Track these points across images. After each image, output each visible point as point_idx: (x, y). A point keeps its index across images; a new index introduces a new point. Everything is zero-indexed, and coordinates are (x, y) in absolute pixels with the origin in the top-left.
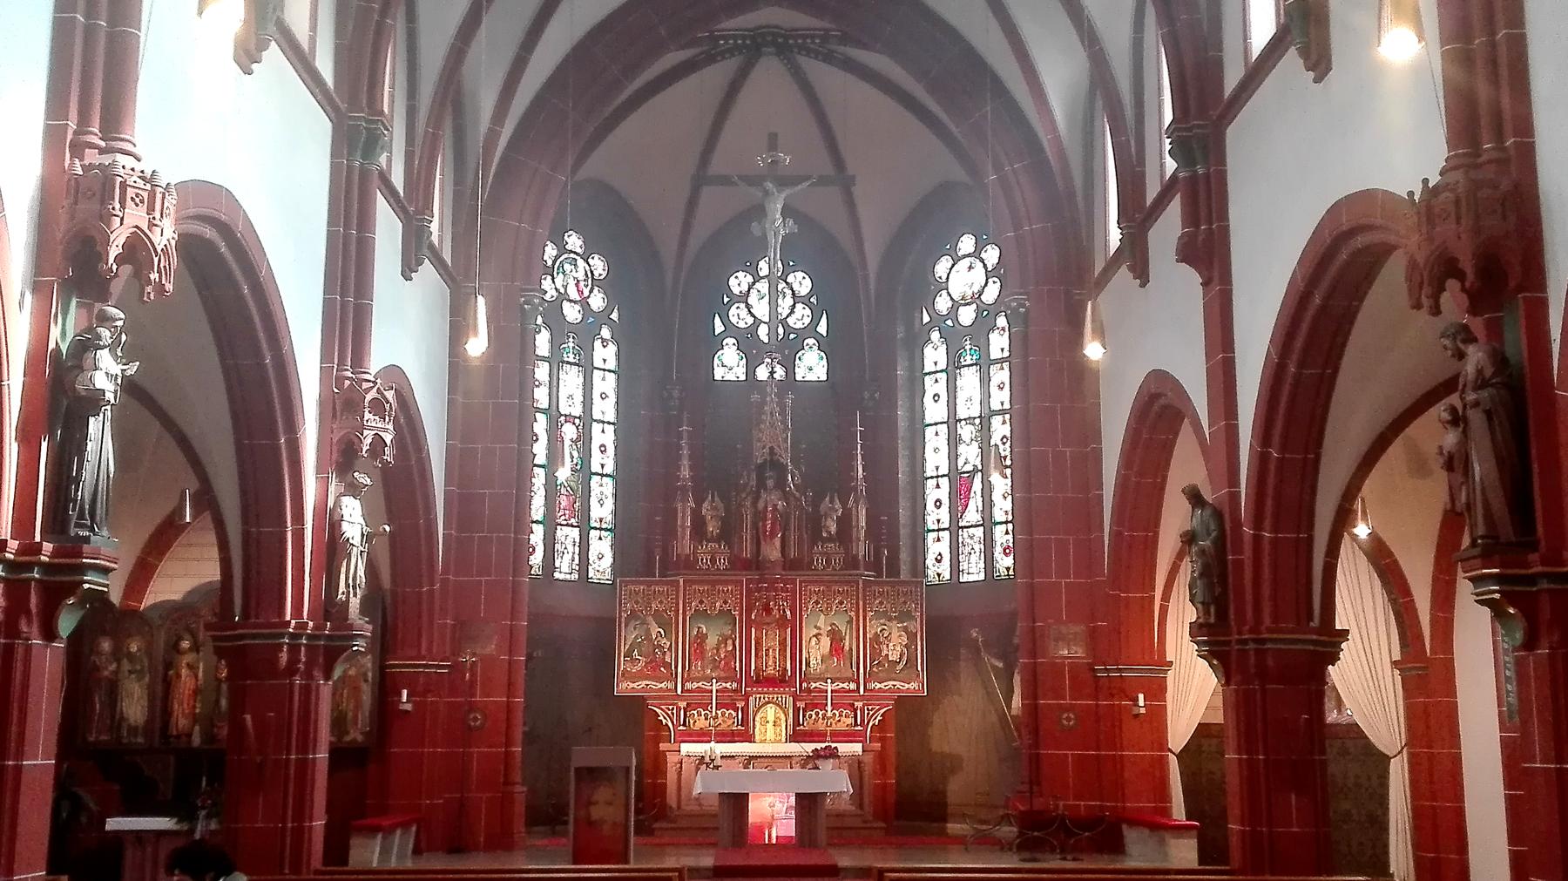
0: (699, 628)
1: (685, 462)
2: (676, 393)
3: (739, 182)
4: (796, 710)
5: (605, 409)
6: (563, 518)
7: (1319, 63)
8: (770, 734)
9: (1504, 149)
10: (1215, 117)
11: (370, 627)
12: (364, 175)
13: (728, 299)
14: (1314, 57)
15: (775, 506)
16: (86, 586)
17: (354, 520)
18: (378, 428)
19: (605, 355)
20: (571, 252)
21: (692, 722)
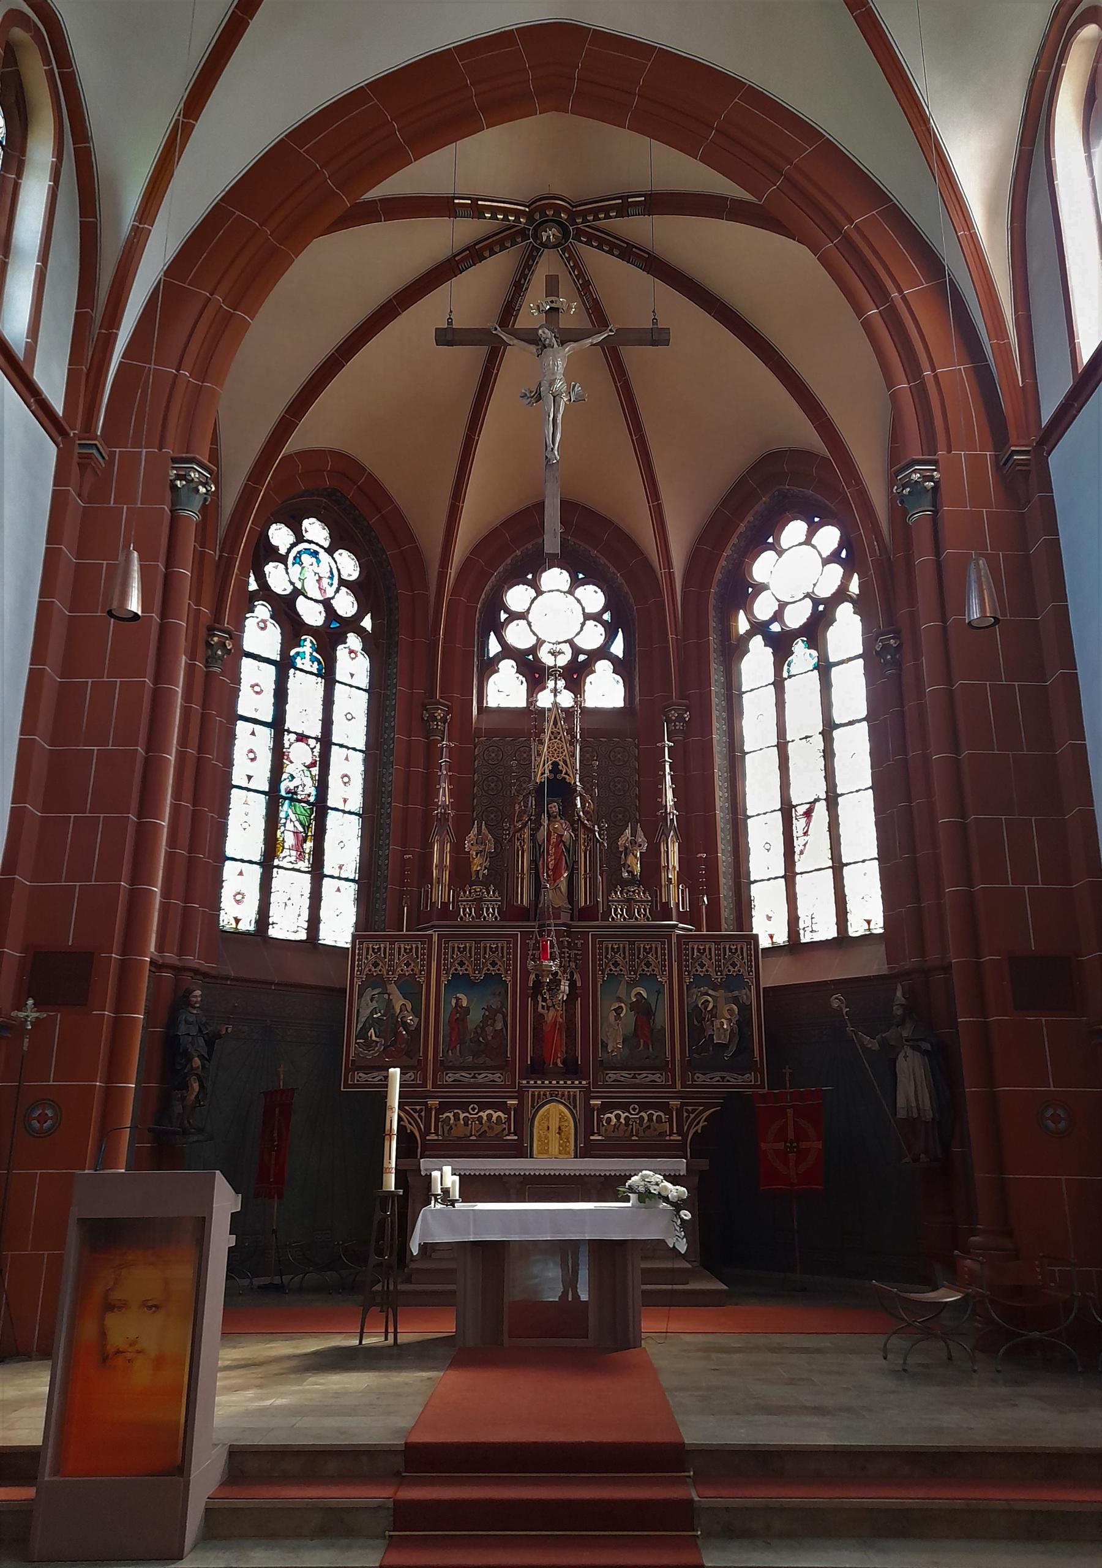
0: (458, 999)
2: (439, 714)
4: (589, 1110)
6: (288, 859)
8: (554, 1148)
13: (507, 616)
21: (446, 1128)
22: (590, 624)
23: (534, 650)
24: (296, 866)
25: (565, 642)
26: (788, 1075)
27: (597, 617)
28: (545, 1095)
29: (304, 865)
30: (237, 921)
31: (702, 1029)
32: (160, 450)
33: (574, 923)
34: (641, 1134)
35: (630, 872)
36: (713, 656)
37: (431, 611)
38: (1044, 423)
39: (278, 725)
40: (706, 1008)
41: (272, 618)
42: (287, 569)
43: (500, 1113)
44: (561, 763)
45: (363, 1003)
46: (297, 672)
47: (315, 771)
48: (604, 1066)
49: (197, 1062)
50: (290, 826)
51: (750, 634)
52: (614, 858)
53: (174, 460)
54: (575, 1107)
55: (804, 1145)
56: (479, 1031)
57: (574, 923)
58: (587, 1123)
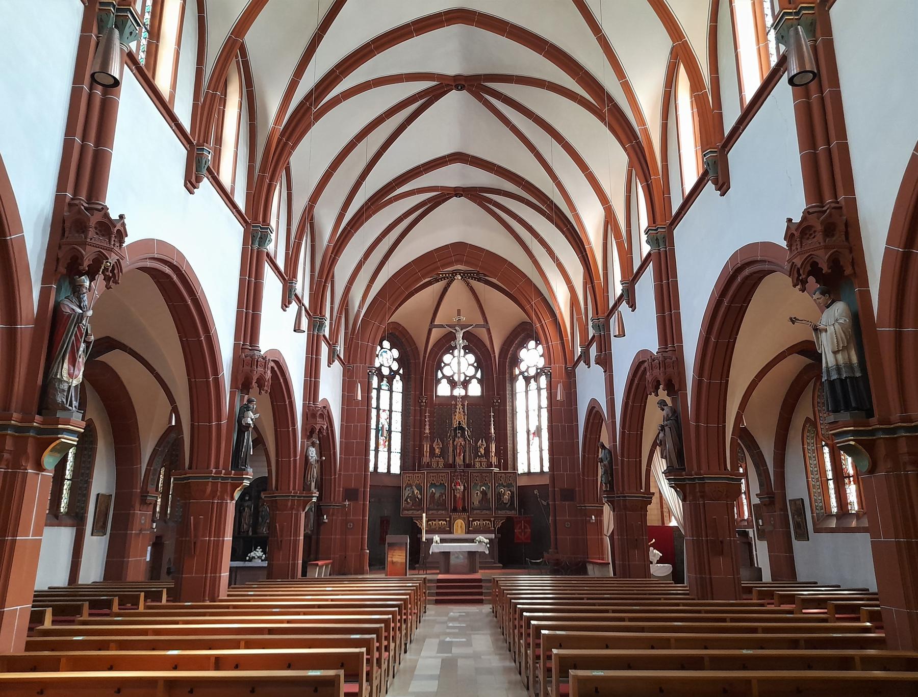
1: (427, 427)
2: (424, 401)
4: (469, 521)
5: (398, 406)
7: (723, 186)
9: (838, 203)
10: (720, 147)
11: (318, 493)
12: (259, 253)
14: (720, 182)
15: (461, 443)
16: (244, 484)
17: (313, 453)
18: (322, 424)
19: (398, 385)
22: (471, 367)
23: (452, 376)
27: (472, 365)
35: (481, 453)
38: (674, 213)
43: (444, 522)
47: (388, 420)
48: (473, 509)
52: (477, 449)
58: (468, 525)
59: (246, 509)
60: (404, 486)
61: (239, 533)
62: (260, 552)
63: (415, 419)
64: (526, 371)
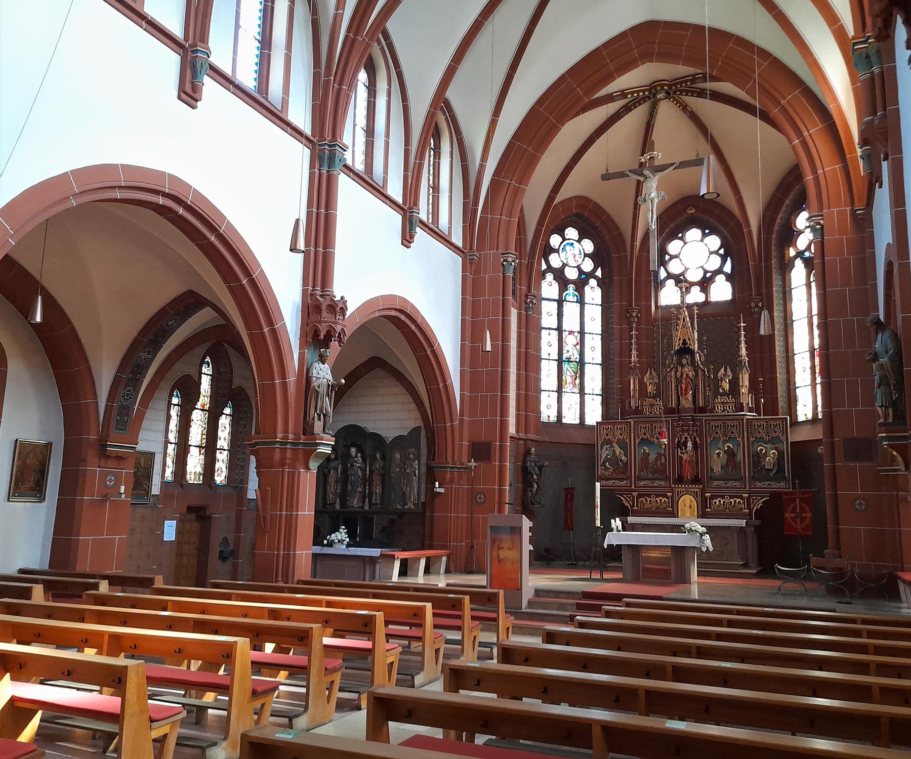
2: (634, 314)
3: (630, 174)
8: (688, 514)
13: (669, 257)
19: (593, 293)
20: (569, 239)
21: (642, 505)
22: (714, 255)
24: (573, 391)
25: (700, 267)
26: (797, 484)
27: (716, 253)
28: (683, 491)
29: (576, 390)
30: (549, 417)
31: (760, 462)
32: (497, 250)
33: (695, 415)
34: (731, 509)
36: (774, 271)
37: (629, 263)
39: (560, 329)
40: (761, 453)
41: (554, 279)
42: (559, 255)
44: (687, 340)
45: (603, 452)
46: (567, 303)
47: (578, 347)
48: (712, 479)
49: (535, 477)
50: (568, 373)
51: (796, 257)
52: (717, 383)
53: (502, 254)
54: (697, 497)
55: (804, 515)
56: (654, 463)
57: (695, 415)
59: (332, 471)
60: (600, 443)
61: (325, 504)
62: (343, 534)
63: (621, 344)
64: (806, 250)
